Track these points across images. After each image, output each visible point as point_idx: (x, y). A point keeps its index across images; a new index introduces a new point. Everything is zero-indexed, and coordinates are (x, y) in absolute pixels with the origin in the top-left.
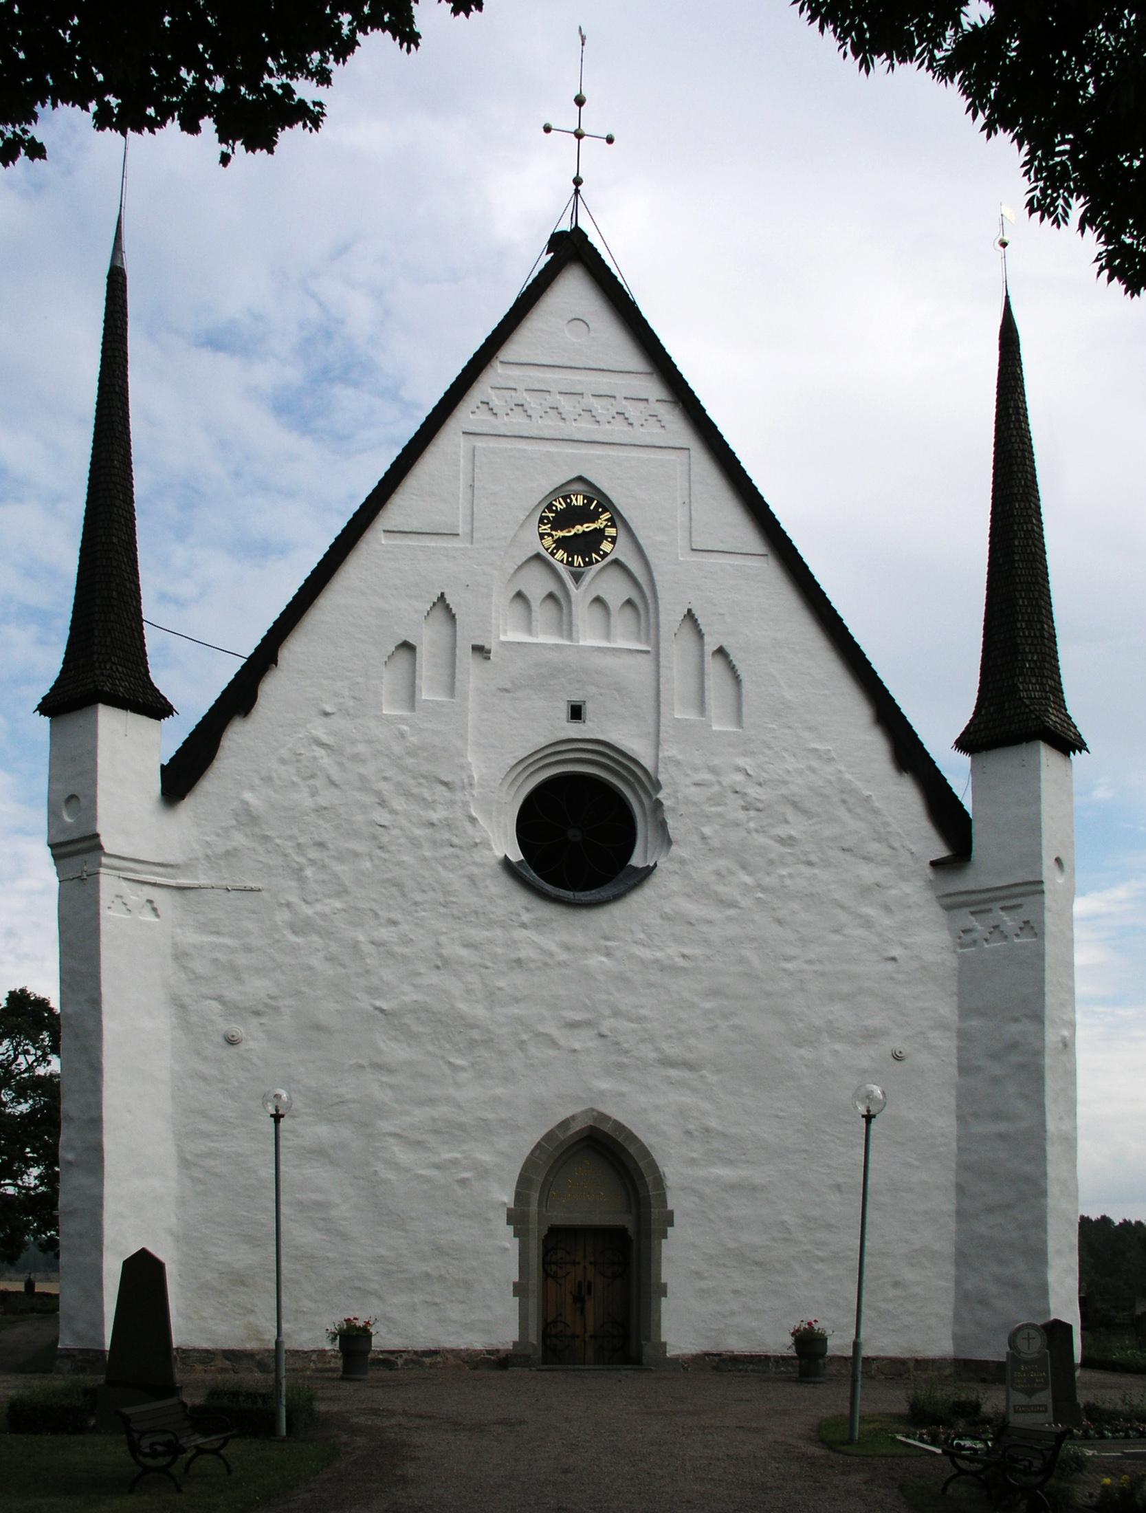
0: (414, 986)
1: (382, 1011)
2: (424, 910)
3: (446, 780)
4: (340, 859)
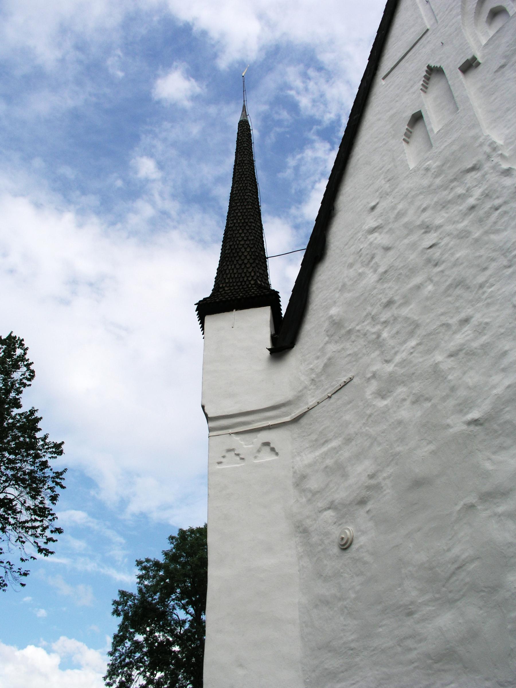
0: (504, 370)
1: (475, 422)
2: (492, 285)
3: (470, 166)
4: (406, 302)
